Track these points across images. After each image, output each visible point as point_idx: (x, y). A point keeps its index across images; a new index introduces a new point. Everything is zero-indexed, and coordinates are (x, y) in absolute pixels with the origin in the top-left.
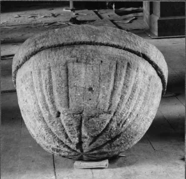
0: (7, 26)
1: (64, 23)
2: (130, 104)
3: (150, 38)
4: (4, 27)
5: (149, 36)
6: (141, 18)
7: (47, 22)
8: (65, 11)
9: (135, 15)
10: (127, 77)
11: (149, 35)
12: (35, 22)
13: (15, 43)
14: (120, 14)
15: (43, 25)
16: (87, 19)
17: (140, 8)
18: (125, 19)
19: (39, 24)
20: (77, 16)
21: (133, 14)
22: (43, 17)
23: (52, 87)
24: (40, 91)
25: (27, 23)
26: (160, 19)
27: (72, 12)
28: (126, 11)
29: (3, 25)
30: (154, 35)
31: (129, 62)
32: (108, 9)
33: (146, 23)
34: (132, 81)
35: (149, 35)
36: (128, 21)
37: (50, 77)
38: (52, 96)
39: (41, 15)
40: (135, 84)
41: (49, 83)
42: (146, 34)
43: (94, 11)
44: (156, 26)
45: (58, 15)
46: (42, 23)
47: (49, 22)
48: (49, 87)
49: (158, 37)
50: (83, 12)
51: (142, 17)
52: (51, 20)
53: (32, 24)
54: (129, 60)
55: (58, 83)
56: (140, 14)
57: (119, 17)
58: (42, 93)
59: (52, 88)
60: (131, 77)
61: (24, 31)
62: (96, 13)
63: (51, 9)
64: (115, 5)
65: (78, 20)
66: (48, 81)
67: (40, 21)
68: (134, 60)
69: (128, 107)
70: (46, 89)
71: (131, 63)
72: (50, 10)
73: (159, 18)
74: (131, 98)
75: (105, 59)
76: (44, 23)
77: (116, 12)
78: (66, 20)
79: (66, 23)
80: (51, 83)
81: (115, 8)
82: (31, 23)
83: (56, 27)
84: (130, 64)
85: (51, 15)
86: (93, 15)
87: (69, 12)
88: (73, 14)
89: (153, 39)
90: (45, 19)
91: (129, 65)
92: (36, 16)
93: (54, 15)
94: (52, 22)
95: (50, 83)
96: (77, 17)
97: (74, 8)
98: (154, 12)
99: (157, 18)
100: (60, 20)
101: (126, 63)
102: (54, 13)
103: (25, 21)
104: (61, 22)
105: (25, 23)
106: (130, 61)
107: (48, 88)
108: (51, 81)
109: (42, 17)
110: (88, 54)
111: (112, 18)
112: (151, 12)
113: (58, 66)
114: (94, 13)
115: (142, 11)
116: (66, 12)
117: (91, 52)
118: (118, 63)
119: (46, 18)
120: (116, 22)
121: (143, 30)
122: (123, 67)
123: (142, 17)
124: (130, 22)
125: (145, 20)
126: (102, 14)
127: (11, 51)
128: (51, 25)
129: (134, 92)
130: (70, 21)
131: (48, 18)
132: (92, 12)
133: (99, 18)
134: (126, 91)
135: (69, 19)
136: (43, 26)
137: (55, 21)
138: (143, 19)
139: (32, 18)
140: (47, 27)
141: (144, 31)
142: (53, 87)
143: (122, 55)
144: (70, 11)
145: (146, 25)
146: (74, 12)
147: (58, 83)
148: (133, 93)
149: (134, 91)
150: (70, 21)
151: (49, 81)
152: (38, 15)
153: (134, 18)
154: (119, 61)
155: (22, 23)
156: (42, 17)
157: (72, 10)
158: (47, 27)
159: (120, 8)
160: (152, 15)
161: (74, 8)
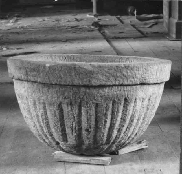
0: (31, 28)
1: (86, 27)
2: (128, 132)
3: (168, 40)
4: (28, 29)
5: (168, 39)
6: (162, 23)
7: (70, 25)
8: (88, 17)
9: (156, 20)
10: (124, 112)
11: (168, 38)
12: (59, 25)
13: (37, 42)
14: (141, 20)
15: (66, 28)
16: (109, 24)
17: (161, 15)
18: (146, 24)
19: (62, 27)
20: (99, 21)
21: (154, 20)
22: (67, 22)
23: (49, 123)
24: (37, 121)
25: (51, 26)
26: (178, 22)
27: (95, 17)
28: (148, 18)
29: (28, 27)
30: (172, 37)
31: (127, 97)
32: (130, 15)
33: (166, 27)
34: (130, 113)
35: (168, 38)
36: (149, 26)
37: (46, 114)
38: (50, 130)
39: (65, 19)
40: (133, 115)
41: (45, 119)
42: (164, 36)
43: (117, 17)
44: (174, 29)
45: (82, 20)
46: (65, 26)
47: (72, 25)
48: (46, 122)
49: (175, 39)
50: (106, 18)
51: (162, 22)
52: (75, 24)
53: (55, 27)
54: (127, 95)
55: (54, 122)
56: (160, 20)
57: (140, 22)
58: (40, 124)
59: (49, 124)
60: (128, 110)
61: (47, 33)
62: (119, 19)
63: (75, 14)
64: (136, 11)
65: (99, 24)
66: (44, 116)
67: (64, 24)
68: (132, 92)
69: (126, 135)
70: (43, 123)
71: (129, 98)
72: (74, 15)
73: (177, 21)
74: (129, 127)
75: (100, 101)
76: (67, 26)
77: (137, 18)
78: (89, 24)
79: (88, 27)
80: (47, 119)
81: (137, 14)
82: (55, 26)
83: (78, 30)
84: (128, 99)
85: (74, 20)
86: (115, 20)
87: (92, 18)
88: (96, 19)
89: (171, 40)
90: (69, 23)
91: (126, 100)
92: (60, 21)
93: (77, 20)
94: (75, 25)
95: (46, 119)
96: (99, 22)
97: (97, 14)
98: (172, 16)
99: (175, 20)
100: (81, 24)
101: (124, 98)
102: (78, 18)
103: (49, 25)
104: (84, 26)
105: (49, 26)
106: (127, 96)
107: (44, 123)
108: (47, 117)
109: (66, 21)
110: (81, 96)
111: (132, 23)
112: (170, 16)
113: (53, 105)
114: (116, 19)
115: (162, 18)
116: (88, 18)
117: (85, 94)
118: (115, 102)
119: (69, 22)
120: (137, 26)
121: (162, 33)
122: (120, 104)
123: (162, 22)
124: (150, 27)
125: (164, 25)
126: (124, 19)
127: (33, 49)
128: (73, 29)
129: (132, 121)
130: (93, 25)
131: (72, 22)
132: (114, 18)
133: (121, 23)
134: (124, 125)
135: (91, 24)
136: (66, 29)
137: (78, 25)
138: (163, 24)
139: (57, 22)
140: (70, 29)
141: (163, 34)
142: (50, 123)
143: (118, 92)
144: (93, 16)
145: (165, 29)
146: (97, 17)
147: (54, 122)
148: (131, 122)
149: (132, 120)
150: (93, 25)
151: (45, 117)
152: (62, 20)
153: (155, 23)
154: (115, 100)
155: (46, 26)
156: (66, 21)
157: (95, 16)
158: (70, 29)
159: (141, 15)
160: (171, 18)
161: (97, 14)
